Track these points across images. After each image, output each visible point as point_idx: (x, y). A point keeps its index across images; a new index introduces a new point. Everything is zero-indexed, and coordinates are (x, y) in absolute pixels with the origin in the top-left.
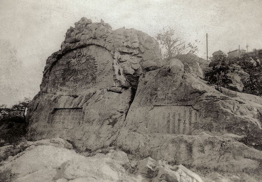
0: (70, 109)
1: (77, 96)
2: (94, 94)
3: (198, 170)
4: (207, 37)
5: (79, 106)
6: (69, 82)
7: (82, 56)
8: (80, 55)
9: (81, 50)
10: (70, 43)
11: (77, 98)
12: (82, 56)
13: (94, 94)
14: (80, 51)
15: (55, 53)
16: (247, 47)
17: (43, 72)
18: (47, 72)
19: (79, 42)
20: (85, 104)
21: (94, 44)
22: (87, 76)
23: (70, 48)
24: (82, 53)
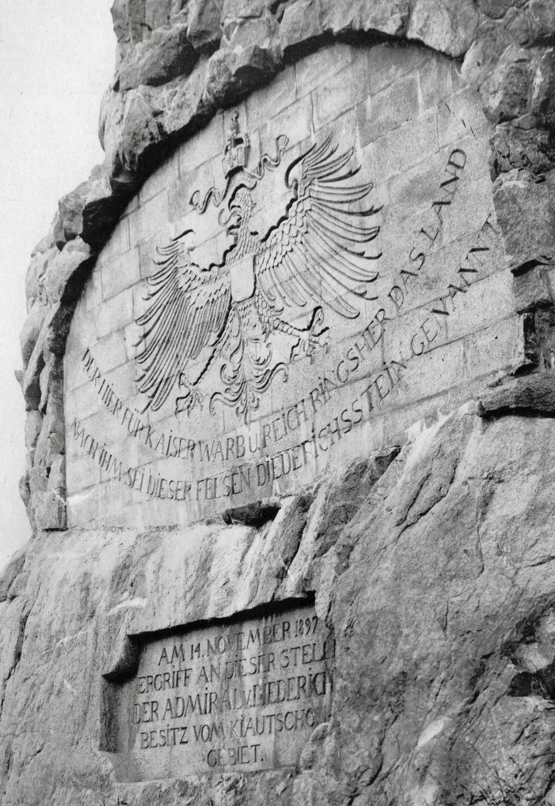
0: (240, 618)
1: (270, 513)
2: (384, 462)
3: (508, 792)
4: (208, 364)
5: (289, 589)
6: (196, 411)
7: (253, 164)
8: (238, 169)
9: (242, 120)
10: (155, 82)
11: (273, 528)
12: (253, 164)
13: (384, 462)
14: (237, 128)
15: (67, 200)
16: (441, 299)
17: (20, 378)
18: (41, 364)
19: (217, 56)
20: (331, 559)
21: (329, 33)
22: (318, 329)
23: (160, 126)
24: (255, 145)
